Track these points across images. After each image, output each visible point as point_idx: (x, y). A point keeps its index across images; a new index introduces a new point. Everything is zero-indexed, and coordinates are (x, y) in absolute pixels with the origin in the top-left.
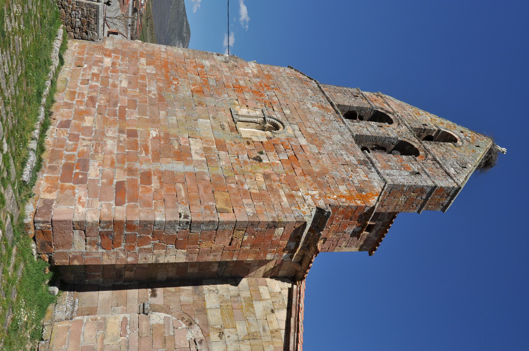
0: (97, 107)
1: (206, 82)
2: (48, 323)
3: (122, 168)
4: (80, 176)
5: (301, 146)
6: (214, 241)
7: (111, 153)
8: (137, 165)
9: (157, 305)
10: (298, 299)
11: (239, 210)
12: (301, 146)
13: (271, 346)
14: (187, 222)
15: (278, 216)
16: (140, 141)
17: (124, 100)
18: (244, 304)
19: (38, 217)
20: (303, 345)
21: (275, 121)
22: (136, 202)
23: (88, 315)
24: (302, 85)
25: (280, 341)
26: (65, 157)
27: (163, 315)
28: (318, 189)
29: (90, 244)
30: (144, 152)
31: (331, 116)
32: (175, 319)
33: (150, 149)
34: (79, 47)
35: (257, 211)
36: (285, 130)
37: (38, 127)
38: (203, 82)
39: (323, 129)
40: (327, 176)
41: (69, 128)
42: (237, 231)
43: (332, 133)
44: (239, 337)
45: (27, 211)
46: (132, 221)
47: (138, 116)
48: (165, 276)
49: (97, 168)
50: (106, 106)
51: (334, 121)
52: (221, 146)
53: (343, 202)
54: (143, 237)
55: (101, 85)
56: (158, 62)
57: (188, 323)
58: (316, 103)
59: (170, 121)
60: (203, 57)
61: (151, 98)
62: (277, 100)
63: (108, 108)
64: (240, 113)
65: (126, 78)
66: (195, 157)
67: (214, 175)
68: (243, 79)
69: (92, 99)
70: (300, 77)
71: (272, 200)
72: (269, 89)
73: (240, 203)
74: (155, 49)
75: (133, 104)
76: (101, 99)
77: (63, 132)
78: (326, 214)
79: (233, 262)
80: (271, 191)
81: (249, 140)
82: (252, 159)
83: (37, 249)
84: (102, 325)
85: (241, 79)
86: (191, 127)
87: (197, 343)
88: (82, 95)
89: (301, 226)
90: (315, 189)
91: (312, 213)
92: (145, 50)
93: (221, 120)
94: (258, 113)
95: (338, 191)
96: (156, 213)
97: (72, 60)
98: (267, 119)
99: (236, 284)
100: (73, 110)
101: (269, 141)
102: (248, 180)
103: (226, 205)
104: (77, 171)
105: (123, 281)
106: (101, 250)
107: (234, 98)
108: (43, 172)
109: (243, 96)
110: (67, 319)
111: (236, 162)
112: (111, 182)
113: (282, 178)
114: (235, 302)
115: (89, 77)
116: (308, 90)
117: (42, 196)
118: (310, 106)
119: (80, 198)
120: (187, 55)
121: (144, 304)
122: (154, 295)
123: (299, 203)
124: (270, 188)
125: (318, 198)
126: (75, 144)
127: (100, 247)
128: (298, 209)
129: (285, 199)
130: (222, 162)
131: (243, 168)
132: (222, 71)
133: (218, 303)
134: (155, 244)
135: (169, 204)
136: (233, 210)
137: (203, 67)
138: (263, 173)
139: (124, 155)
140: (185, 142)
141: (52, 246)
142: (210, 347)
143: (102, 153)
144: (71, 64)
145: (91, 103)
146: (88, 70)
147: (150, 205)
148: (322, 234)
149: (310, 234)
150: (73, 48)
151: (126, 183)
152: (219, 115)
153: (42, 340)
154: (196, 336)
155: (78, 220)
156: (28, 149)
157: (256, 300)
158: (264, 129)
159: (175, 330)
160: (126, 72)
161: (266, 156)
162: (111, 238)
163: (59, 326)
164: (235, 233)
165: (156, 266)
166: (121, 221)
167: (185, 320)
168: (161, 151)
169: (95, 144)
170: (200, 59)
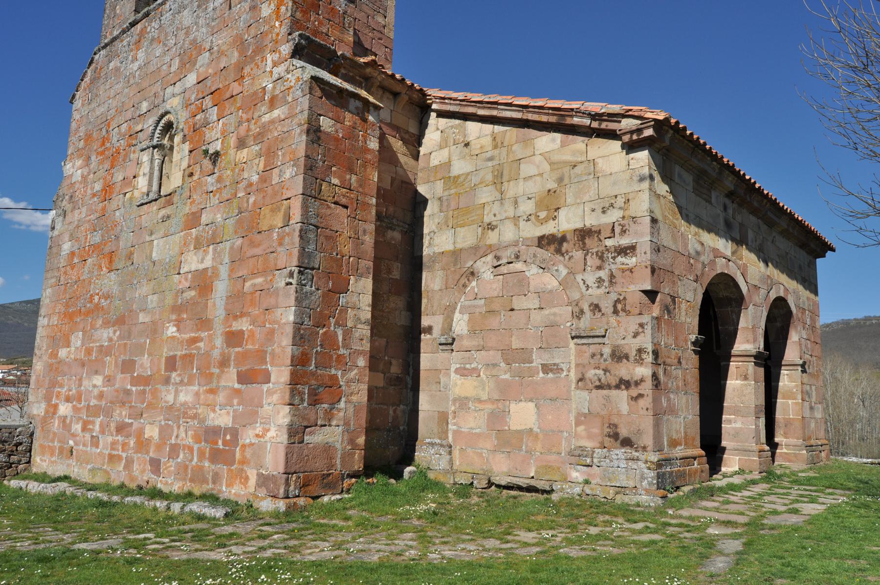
0: (132, 421)
1: (96, 247)
2: (452, 478)
3: (219, 377)
4: (228, 437)
5: (198, 83)
6: (337, 232)
7: (197, 394)
8: (216, 354)
9: (443, 324)
10: (452, 102)
11: (287, 189)
12: (198, 83)
13: (514, 148)
14: (299, 273)
15: (300, 125)
16: (182, 351)
17: (122, 381)
18: (453, 191)
19: (279, 492)
20: (517, 95)
21: (159, 128)
22: (266, 352)
23: (447, 423)
24: (102, 79)
25: (508, 134)
26: (201, 461)
27: (457, 316)
28: (265, 54)
29: (329, 420)
30: (198, 344)
31: (152, 27)
32: (463, 297)
33: (193, 335)
34: (43, 454)
35: (291, 160)
36: (172, 111)
37: (153, 503)
38: (96, 252)
39: (173, 42)
40: (246, 37)
41: (160, 460)
42: (322, 194)
43: (180, 26)
44: (497, 198)
45: (270, 509)
46: (293, 357)
47: (146, 356)
48: (403, 313)
49: (217, 414)
50: (131, 407)
51: (160, 20)
52: (193, 221)
53: (287, 9)
54: (322, 341)
55: (100, 417)
56: (66, 328)
57: (471, 278)
58: (132, 54)
59: (154, 304)
60: (57, 253)
61: (120, 338)
62: (126, 124)
63: (133, 404)
64: (145, 190)
65: (90, 379)
66: (208, 263)
67: (236, 232)
68: (91, 184)
69: (121, 428)
70: (89, 82)
71: (276, 135)
72: (108, 139)
73: (277, 188)
74: (44, 334)
75: (128, 366)
76: (121, 414)
77: (166, 469)
78: (303, 42)
79: (377, 205)
80: (263, 136)
81: (187, 173)
82: (214, 169)
83: (333, 494)
84: (463, 403)
85: (92, 189)
86: (164, 272)
87: (499, 263)
88: (114, 443)
89: (319, 86)
90: (264, 59)
91: (298, 65)
92: (47, 350)
93: (155, 221)
94: (145, 157)
95: (270, 19)
96: (283, 321)
97: (61, 463)
98: (155, 142)
99: (424, 202)
100: (135, 455)
101: (188, 139)
102: (246, 175)
103: (279, 211)
104: (220, 442)
105: (407, 376)
106: (342, 405)
107: (122, 200)
108: (220, 491)
109: (119, 185)
110: (450, 453)
111: (218, 196)
112: (238, 392)
113: (244, 116)
114: (448, 206)
115: (88, 436)
116: (110, 68)
117: (252, 490)
118: (136, 66)
119: (257, 436)
120: (53, 280)
121: (440, 344)
122: (429, 330)
123: (283, 88)
124: (259, 137)
125: (277, 55)
126: (184, 450)
127: (336, 406)
128: (291, 91)
129: (276, 113)
130: (217, 219)
131: (228, 184)
132: (79, 221)
133: (447, 232)
134: (337, 324)
135: (272, 301)
136: (286, 200)
137: (73, 254)
138: (235, 150)
139: (201, 374)
140: (186, 279)
141: (330, 474)
142: (505, 244)
143: (196, 409)
144: (68, 465)
145: (126, 429)
146: (78, 438)
147: (272, 332)
148: (341, 52)
149: (342, 73)
150: (45, 464)
151: (240, 369)
152: (146, 225)
153: (472, 483)
154: (489, 266)
155: (286, 436)
156: (182, 513)
157: (449, 172)
158: (172, 148)
159: (479, 297)
160: (80, 380)
161: (211, 144)
162: (321, 389)
163: (458, 463)
164: (325, 198)
165: (377, 324)
166: (292, 374)
167: (467, 282)
168: (198, 317)
169: (184, 420)
170: (59, 259)
